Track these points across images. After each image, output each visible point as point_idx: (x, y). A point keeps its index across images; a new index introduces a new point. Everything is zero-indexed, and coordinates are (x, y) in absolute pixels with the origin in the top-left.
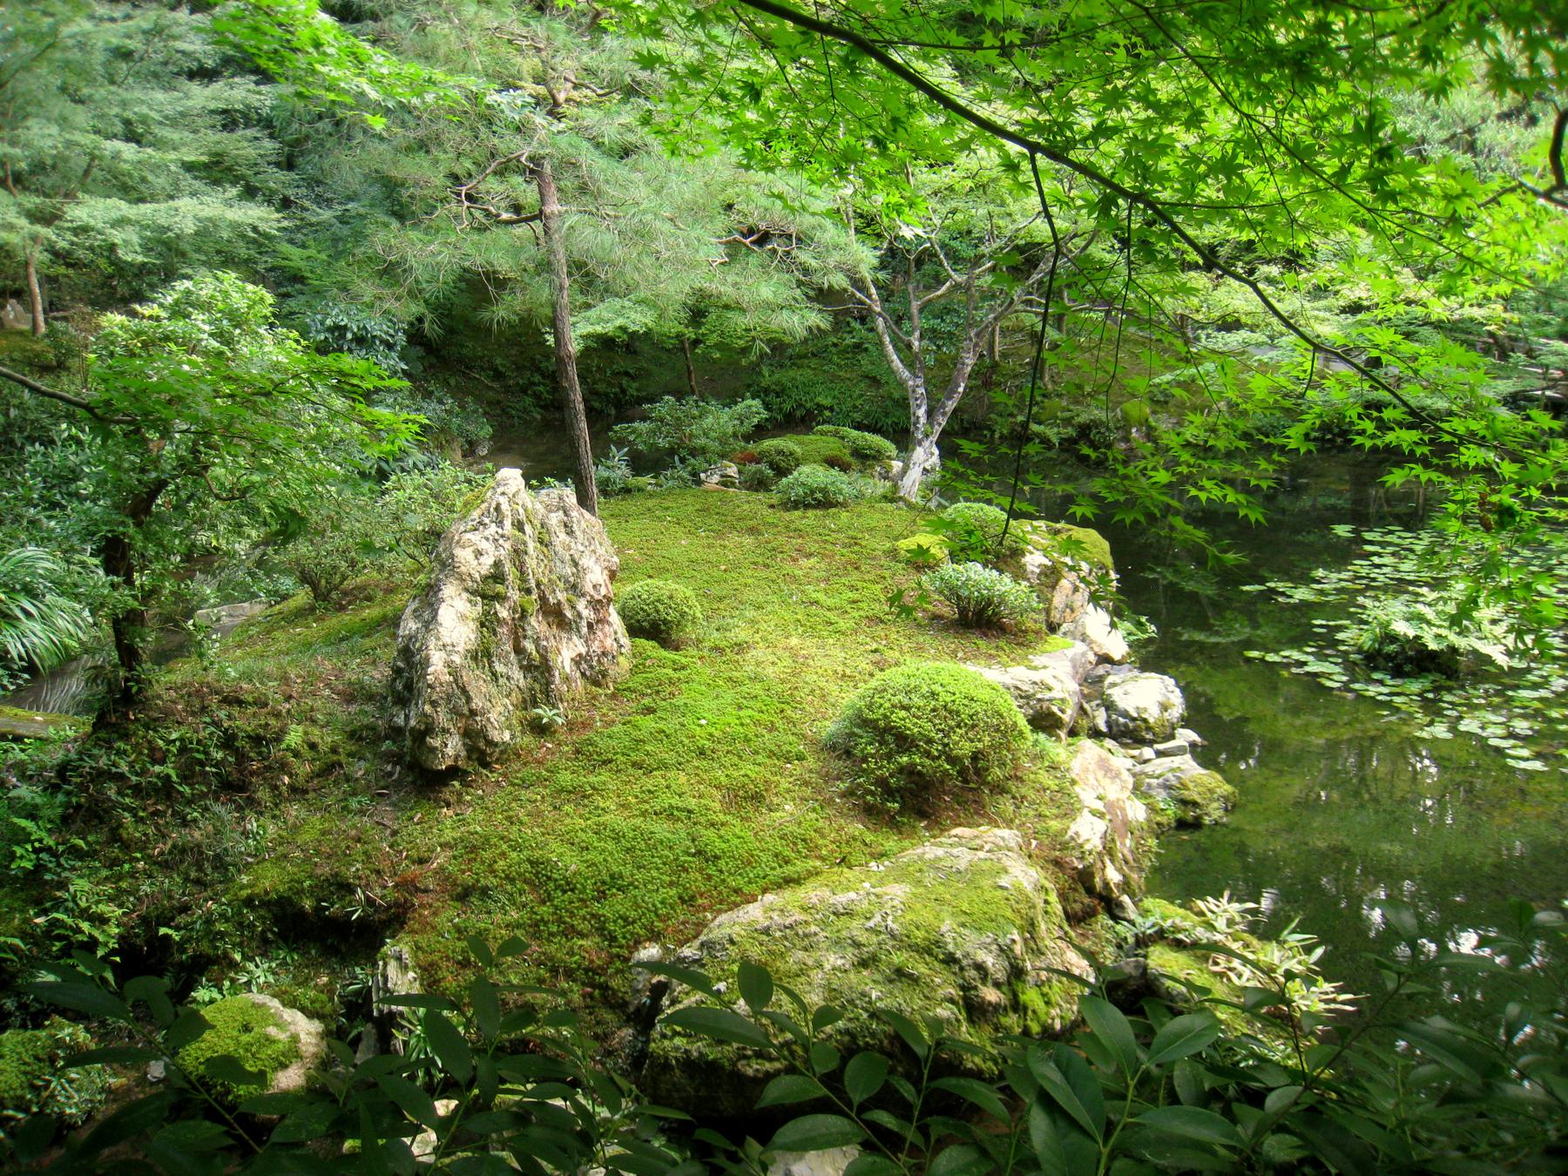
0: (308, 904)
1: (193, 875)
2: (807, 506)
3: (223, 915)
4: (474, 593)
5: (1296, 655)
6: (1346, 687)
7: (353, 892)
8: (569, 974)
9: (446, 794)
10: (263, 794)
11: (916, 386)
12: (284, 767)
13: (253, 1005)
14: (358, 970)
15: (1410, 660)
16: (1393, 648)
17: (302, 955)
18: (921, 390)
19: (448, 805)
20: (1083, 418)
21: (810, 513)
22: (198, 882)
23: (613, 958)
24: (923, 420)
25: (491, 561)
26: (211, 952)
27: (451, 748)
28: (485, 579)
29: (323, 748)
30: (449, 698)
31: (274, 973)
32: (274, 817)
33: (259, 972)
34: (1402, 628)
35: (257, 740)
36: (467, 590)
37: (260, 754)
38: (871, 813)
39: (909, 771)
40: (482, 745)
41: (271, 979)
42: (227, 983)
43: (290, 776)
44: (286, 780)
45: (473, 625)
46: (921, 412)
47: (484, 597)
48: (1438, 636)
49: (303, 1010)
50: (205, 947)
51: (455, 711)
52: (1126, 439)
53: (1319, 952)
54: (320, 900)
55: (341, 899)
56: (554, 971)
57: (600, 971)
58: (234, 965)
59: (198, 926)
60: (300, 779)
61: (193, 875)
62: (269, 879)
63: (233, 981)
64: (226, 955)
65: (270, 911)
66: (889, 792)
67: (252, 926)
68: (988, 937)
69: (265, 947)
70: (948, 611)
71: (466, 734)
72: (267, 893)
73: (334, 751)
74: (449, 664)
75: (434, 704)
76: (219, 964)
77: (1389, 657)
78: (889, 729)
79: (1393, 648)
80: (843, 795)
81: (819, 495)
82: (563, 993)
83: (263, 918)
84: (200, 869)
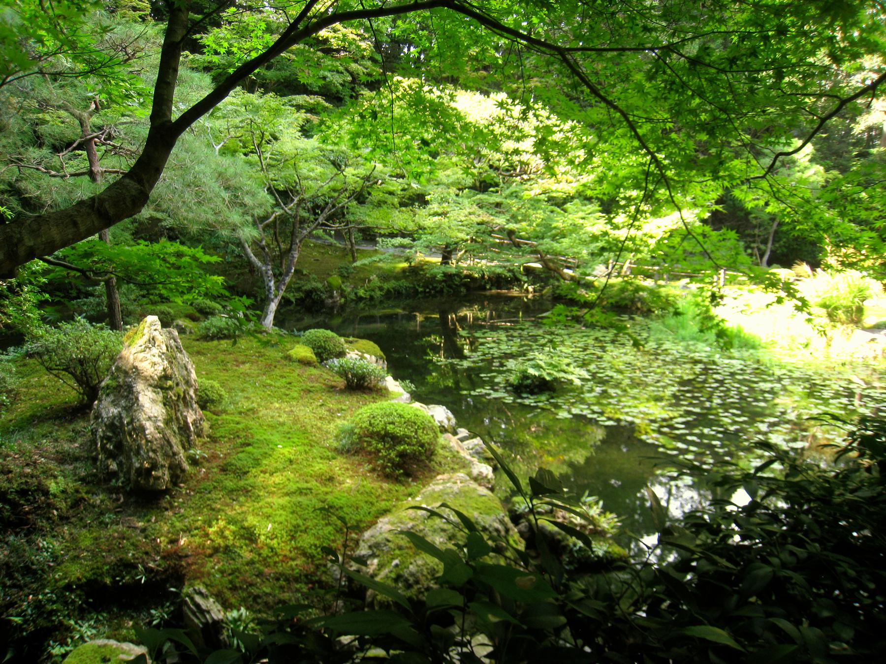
0: (108, 581)
1: (9, 583)
2: (219, 339)
3: (50, 600)
4: (156, 387)
5: (484, 391)
6: (514, 402)
7: (137, 568)
8: (297, 580)
9: (164, 503)
10: (42, 523)
11: (268, 270)
12: (50, 506)
13: (99, 647)
14: (153, 612)
15: (537, 386)
16: (529, 381)
17: (109, 613)
18: (270, 272)
19: (167, 509)
20: (308, 287)
21: (222, 342)
22: (14, 586)
23: (317, 567)
24: (273, 288)
25: (161, 368)
26: (49, 624)
27: (164, 475)
28: (160, 378)
29: (69, 491)
30: (162, 447)
31: (94, 628)
32: (54, 536)
33: (83, 629)
34: (532, 371)
35: (23, 493)
36: (150, 385)
37: (27, 500)
38: (387, 477)
39: (402, 455)
40: (179, 472)
41: (94, 631)
42: (69, 640)
43: (57, 510)
44: (55, 512)
45: (161, 405)
46: (272, 284)
47: (162, 388)
48: (549, 374)
49: (132, 641)
50: (41, 622)
51: (166, 455)
52: (332, 297)
53: (601, 503)
54: (114, 577)
55: (128, 573)
56: (287, 580)
57: (314, 574)
58: (69, 629)
59: (29, 611)
60: (64, 510)
61: (9, 583)
62: (76, 572)
63: (72, 638)
64: (61, 623)
65: (82, 590)
66: (397, 466)
67: (73, 602)
68: (493, 517)
69: (82, 614)
70: (341, 382)
71: (171, 467)
72: (79, 579)
73: (77, 491)
74: (157, 428)
75: (154, 451)
76: (59, 630)
77: (527, 386)
78: (387, 434)
79: (529, 381)
80: (370, 471)
81: (225, 332)
82: (298, 590)
83: (79, 596)
84: (11, 577)
